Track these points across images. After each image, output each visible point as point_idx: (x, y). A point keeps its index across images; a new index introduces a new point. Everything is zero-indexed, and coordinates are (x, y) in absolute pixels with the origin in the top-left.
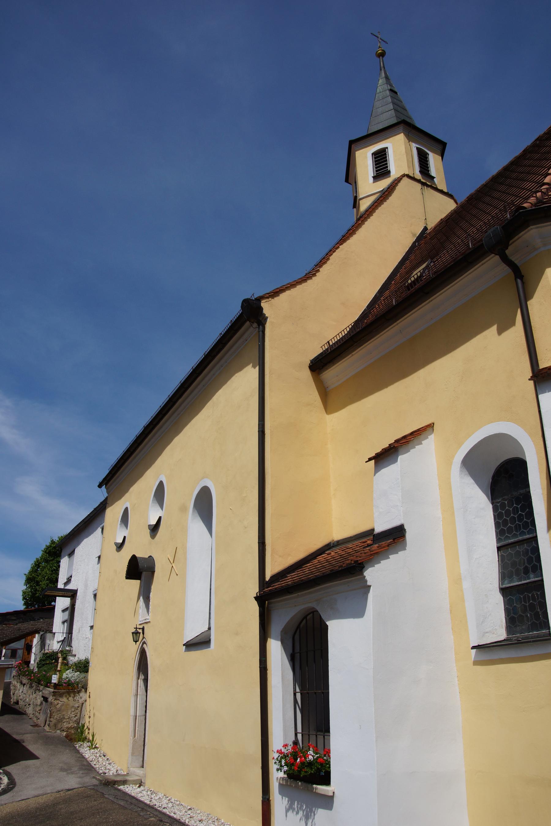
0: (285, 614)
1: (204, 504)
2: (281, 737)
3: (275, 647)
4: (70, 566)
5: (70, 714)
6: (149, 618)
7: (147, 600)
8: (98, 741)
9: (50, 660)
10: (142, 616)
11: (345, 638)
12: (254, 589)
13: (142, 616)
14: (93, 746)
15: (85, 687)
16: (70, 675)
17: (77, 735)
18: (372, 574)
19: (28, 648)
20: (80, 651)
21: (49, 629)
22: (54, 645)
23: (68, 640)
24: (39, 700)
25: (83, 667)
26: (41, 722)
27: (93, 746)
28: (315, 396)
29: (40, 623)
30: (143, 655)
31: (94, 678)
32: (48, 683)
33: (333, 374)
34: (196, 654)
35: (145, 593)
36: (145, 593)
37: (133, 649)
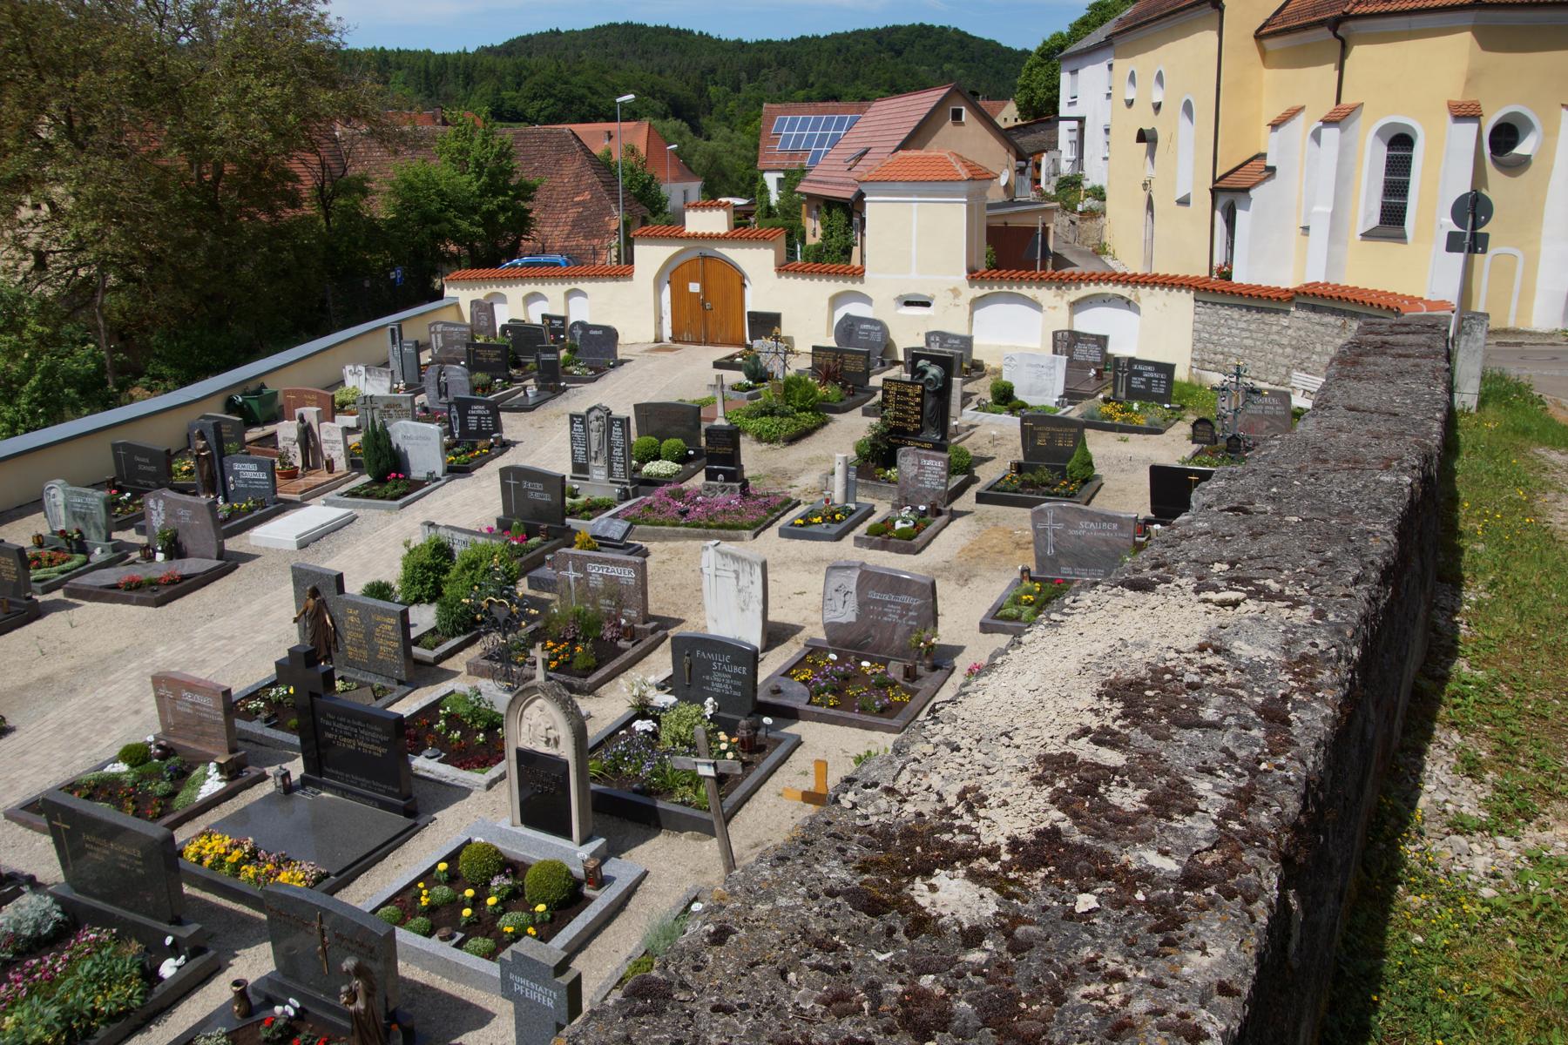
0: (1223, 200)
1: (1188, 108)
2: (1219, 260)
3: (1218, 215)
4: (1074, 85)
5: (1094, 234)
6: (1154, 174)
7: (1152, 158)
8: (1117, 255)
9: (1070, 184)
10: (1149, 172)
11: (1241, 215)
12: (1210, 184)
13: (1149, 172)
14: (1114, 259)
15: (1104, 214)
16: (1089, 203)
17: (1100, 250)
18: (1252, 193)
19: (1038, 166)
20: (1094, 174)
21: (1054, 145)
22: (1066, 169)
23: (1079, 159)
24: (1067, 223)
25: (1099, 194)
26: (1071, 238)
27: (1114, 259)
28: (1257, 56)
29: (1042, 136)
30: (1150, 198)
31: (1110, 205)
32: (1074, 211)
33: (1269, 43)
34: (1182, 208)
35: (1151, 153)
36: (1151, 153)
37: (1143, 196)
